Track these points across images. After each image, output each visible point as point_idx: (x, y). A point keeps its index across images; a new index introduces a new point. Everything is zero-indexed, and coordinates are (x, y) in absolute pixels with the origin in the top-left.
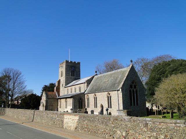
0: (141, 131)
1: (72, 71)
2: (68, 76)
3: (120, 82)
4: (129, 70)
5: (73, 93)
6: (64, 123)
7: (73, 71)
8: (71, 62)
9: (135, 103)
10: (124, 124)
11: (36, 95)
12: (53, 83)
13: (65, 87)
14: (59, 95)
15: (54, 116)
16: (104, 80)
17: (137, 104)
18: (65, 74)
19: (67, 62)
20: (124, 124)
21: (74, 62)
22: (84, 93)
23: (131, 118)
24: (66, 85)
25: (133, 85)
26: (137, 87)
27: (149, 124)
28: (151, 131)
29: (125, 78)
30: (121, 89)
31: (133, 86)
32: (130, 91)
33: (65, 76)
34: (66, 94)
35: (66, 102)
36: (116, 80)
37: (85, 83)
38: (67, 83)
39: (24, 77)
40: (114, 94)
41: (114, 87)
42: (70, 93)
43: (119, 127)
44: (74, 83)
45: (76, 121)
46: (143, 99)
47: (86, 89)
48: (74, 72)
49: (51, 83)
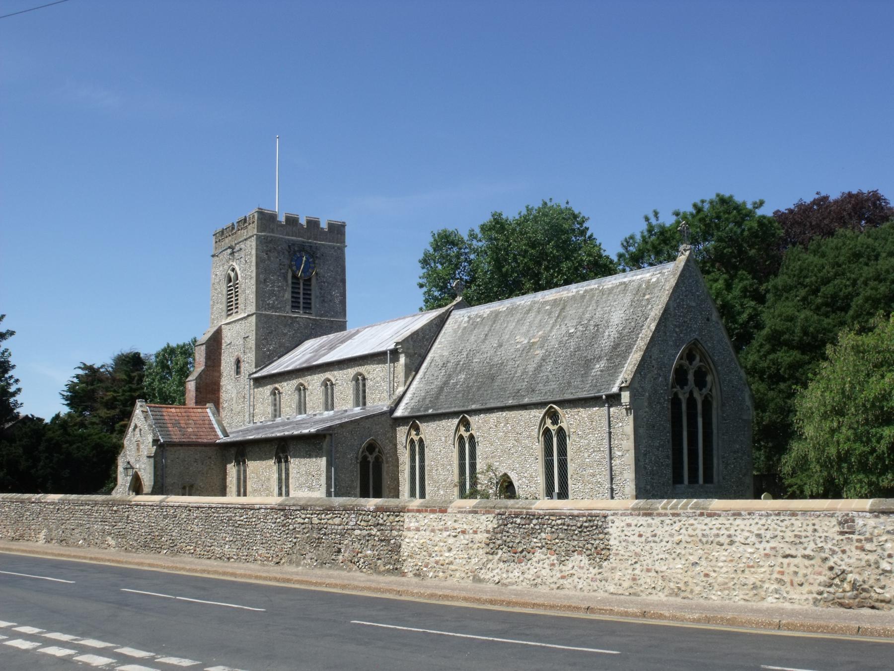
1: (295, 277)
2: (273, 307)
3: (618, 352)
4: (673, 282)
5: (310, 412)
6: (405, 551)
7: (302, 275)
8: (292, 221)
9: (697, 469)
13: (259, 382)
19: (266, 219)
21: (309, 222)
22: (392, 410)
24: (263, 359)
26: (709, 378)
29: (653, 327)
30: (626, 397)
31: (691, 377)
32: (675, 402)
33: (252, 309)
41: (585, 375)
44: (317, 352)
45: (482, 537)
47: (401, 389)
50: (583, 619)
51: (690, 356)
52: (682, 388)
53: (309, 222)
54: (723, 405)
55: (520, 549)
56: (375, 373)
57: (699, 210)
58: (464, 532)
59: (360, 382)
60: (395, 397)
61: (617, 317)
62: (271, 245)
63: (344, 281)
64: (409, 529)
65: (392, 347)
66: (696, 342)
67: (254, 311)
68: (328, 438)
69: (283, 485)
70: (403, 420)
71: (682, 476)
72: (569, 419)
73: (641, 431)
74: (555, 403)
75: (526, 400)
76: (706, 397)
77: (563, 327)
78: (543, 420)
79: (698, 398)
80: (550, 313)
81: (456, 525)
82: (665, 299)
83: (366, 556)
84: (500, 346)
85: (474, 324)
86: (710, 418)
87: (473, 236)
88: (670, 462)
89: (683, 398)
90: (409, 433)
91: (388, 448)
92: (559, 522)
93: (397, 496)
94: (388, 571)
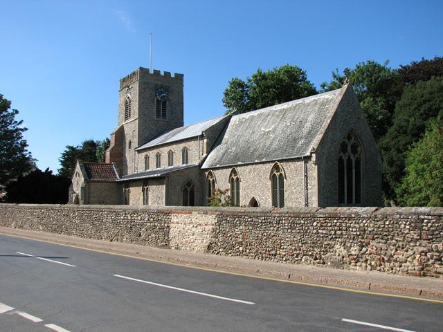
0: (403, 241)
1: (158, 101)
3: (311, 135)
4: (340, 98)
8: (157, 73)
10: (357, 226)
11: (51, 172)
12: (95, 141)
13: (139, 152)
14: (122, 171)
15: (139, 218)
16: (263, 129)
18: (137, 111)
19: (144, 71)
20: (355, 227)
23: (377, 210)
25: (349, 145)
26: (359, 149)
27: (425, 221)
28: (430, 237)
30: (314, 155)
31: (349, 148)
32: (341, 161)
34: (141, 169)
35: (145, 192)
36: (301, 126)
37: (202, 137)
38: (145, 136)
39: (17, 118)
41: (293, 148)
42: (153, 167)
43: (342, 234)
46: (374, 184)
47: (205, 155)
48: (164, 103)
49: (88, 139)
50: (63, 327)
51: (349, 138)
52: (344, 153)
54: (366, 163)
55: (229, 235)
56: (193, 146)
57: (358, 67)
58: (200, 225)
59: (185, 153)
60: (201, 159)
61: (311, 118)
62: (146, 85)
64: (173, 223)
65: (201, 134)
66: (352, 130)
67: (137, 117)
68: (167, 178)
69: (146, 201)
70: (206, 170)
71: (344, 199)
72: (288, 168)
73: (321, 175)
74: (278, 161)
75: (264, 160)
77: (285, 123)
80: (278, 116)
81: (197, 221)
82: (335, 107)
83: (152, 237)
84: (253, 133)
85: (241, 123)
86: (360, 171)
87: (250, 81)
88: (337, 192)
89: (345, 158)
92: (250, 219)
93: (127, 203)
94: (163, 245)
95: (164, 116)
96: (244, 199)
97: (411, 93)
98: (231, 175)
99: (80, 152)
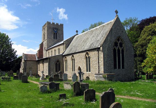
8: (53, 24)
17: (123, 68)
19: (49, 23)
21: (57, 24)
26: (123, 45)
31: (119, 45)
32: (114, 50)
40: (93, 55)
47: (65, 50)
48: (56, 34)
52: (116, 47)
53: (57, 24)
54: (127, 51)
63: (63, 34)
66: (119, 37)
72: (91, 54)
76: (122, 49)
78: (86, 55)
79: (121, 49)
89: (117, 49)
90: (65, 59)
91: (62, 61)
95: (56, 38)
96: (76, 67)
97: (147, 28)
98: (72, 58)
99: (143, 60)
